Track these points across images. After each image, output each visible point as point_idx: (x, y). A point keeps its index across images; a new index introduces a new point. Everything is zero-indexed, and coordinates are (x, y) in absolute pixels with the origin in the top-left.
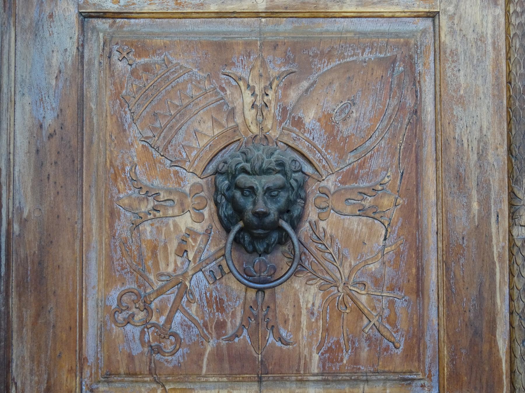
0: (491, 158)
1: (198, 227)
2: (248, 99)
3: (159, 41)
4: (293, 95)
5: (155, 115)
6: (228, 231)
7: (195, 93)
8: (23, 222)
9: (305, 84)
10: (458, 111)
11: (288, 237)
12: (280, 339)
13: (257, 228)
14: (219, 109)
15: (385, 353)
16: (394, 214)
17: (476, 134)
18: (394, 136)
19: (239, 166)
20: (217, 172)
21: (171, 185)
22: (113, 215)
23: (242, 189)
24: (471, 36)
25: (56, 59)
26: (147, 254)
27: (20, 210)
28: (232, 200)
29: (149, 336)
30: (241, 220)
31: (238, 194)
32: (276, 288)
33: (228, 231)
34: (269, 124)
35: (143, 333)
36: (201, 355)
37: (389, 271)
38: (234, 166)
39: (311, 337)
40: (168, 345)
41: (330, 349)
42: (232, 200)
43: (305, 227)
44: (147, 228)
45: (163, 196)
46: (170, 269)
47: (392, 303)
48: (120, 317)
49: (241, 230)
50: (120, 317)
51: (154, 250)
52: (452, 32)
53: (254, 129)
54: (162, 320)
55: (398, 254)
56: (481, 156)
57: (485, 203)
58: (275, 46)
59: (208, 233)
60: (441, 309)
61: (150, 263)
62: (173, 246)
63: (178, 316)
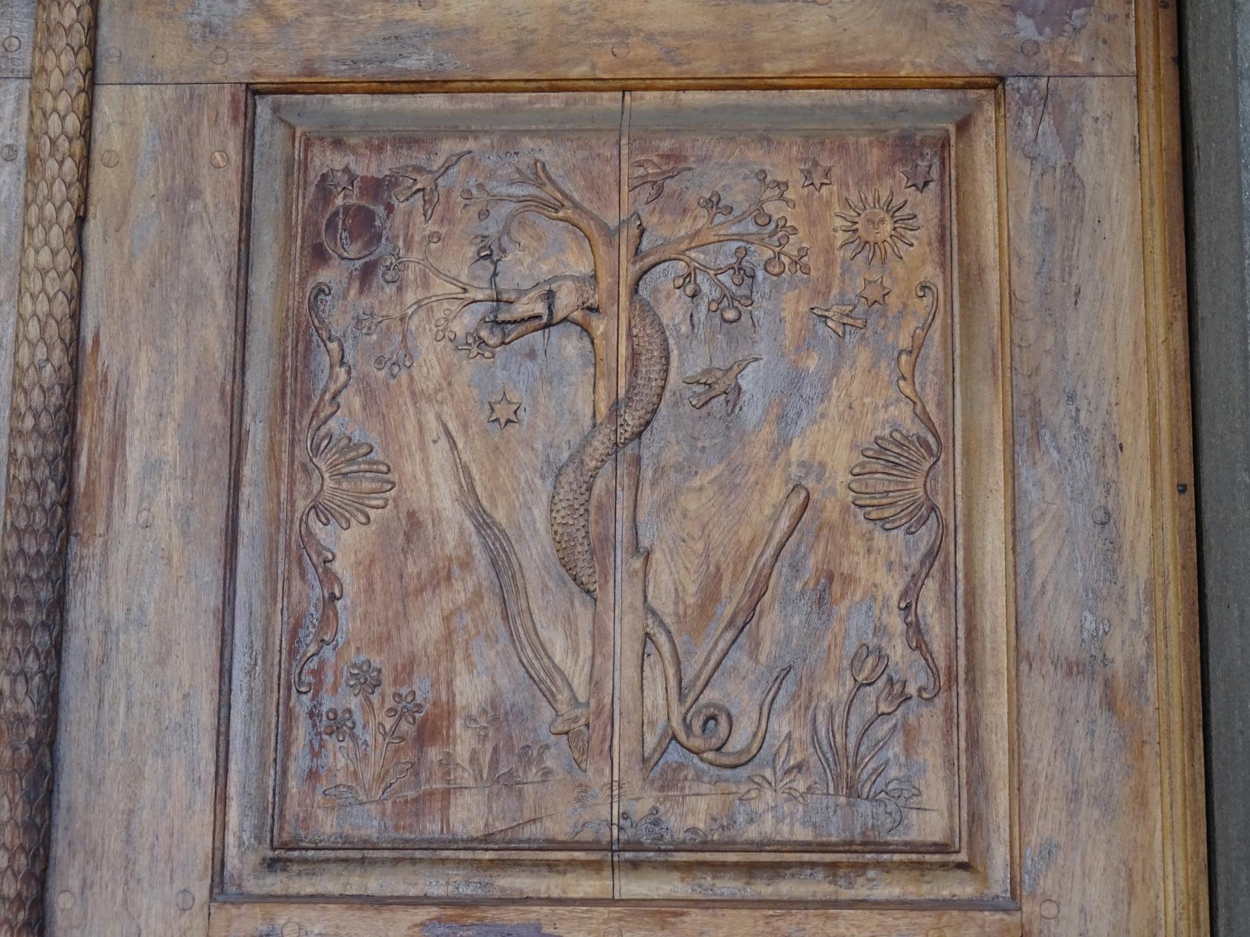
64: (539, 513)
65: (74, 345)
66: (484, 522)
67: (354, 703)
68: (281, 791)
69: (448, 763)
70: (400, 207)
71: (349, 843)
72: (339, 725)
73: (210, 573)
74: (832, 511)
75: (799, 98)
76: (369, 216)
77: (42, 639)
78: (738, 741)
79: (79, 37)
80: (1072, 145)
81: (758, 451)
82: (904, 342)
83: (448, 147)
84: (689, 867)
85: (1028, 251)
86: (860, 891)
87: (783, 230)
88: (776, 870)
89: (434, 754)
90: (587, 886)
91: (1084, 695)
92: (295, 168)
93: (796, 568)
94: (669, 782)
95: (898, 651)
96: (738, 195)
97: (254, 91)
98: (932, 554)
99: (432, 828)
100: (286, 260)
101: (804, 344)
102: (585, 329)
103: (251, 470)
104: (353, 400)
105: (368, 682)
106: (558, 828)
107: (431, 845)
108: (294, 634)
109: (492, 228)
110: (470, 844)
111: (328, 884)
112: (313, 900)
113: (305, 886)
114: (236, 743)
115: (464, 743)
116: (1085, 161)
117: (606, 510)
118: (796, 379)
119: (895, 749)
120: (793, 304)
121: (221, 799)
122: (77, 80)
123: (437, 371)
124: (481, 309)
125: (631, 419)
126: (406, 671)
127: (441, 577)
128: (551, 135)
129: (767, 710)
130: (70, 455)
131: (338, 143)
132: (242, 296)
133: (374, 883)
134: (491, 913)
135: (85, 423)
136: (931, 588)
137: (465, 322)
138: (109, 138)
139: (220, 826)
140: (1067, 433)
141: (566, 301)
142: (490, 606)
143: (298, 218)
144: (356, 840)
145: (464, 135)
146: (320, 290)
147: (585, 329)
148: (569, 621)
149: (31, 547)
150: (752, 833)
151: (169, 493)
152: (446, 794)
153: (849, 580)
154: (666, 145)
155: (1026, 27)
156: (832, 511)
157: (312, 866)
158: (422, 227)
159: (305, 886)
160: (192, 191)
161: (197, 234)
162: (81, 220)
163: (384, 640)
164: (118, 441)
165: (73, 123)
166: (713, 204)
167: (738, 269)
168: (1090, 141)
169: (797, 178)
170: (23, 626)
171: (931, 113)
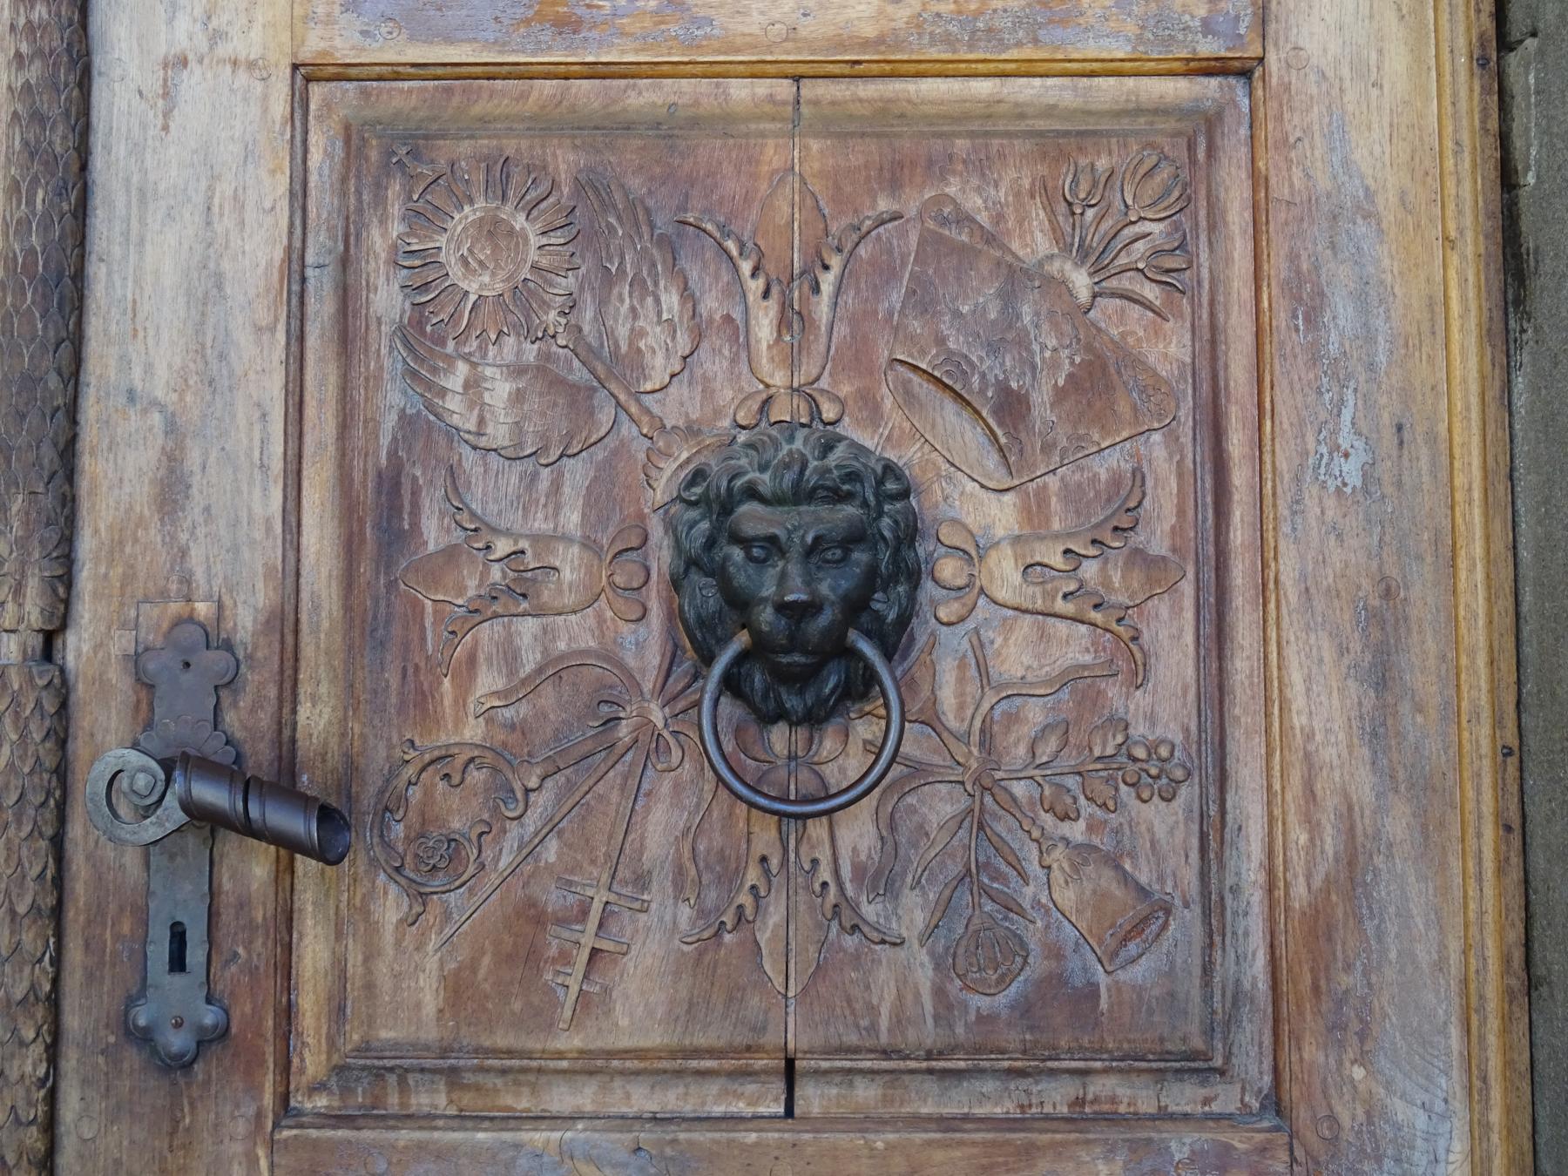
13: (787, 651)
15: (1419, 719)
19: (738, 483)
23: (745, 542)
30: (744, 627)
32: (810, 822)
38: (724, 484)
49: (742, 657)
60: (377, 68)
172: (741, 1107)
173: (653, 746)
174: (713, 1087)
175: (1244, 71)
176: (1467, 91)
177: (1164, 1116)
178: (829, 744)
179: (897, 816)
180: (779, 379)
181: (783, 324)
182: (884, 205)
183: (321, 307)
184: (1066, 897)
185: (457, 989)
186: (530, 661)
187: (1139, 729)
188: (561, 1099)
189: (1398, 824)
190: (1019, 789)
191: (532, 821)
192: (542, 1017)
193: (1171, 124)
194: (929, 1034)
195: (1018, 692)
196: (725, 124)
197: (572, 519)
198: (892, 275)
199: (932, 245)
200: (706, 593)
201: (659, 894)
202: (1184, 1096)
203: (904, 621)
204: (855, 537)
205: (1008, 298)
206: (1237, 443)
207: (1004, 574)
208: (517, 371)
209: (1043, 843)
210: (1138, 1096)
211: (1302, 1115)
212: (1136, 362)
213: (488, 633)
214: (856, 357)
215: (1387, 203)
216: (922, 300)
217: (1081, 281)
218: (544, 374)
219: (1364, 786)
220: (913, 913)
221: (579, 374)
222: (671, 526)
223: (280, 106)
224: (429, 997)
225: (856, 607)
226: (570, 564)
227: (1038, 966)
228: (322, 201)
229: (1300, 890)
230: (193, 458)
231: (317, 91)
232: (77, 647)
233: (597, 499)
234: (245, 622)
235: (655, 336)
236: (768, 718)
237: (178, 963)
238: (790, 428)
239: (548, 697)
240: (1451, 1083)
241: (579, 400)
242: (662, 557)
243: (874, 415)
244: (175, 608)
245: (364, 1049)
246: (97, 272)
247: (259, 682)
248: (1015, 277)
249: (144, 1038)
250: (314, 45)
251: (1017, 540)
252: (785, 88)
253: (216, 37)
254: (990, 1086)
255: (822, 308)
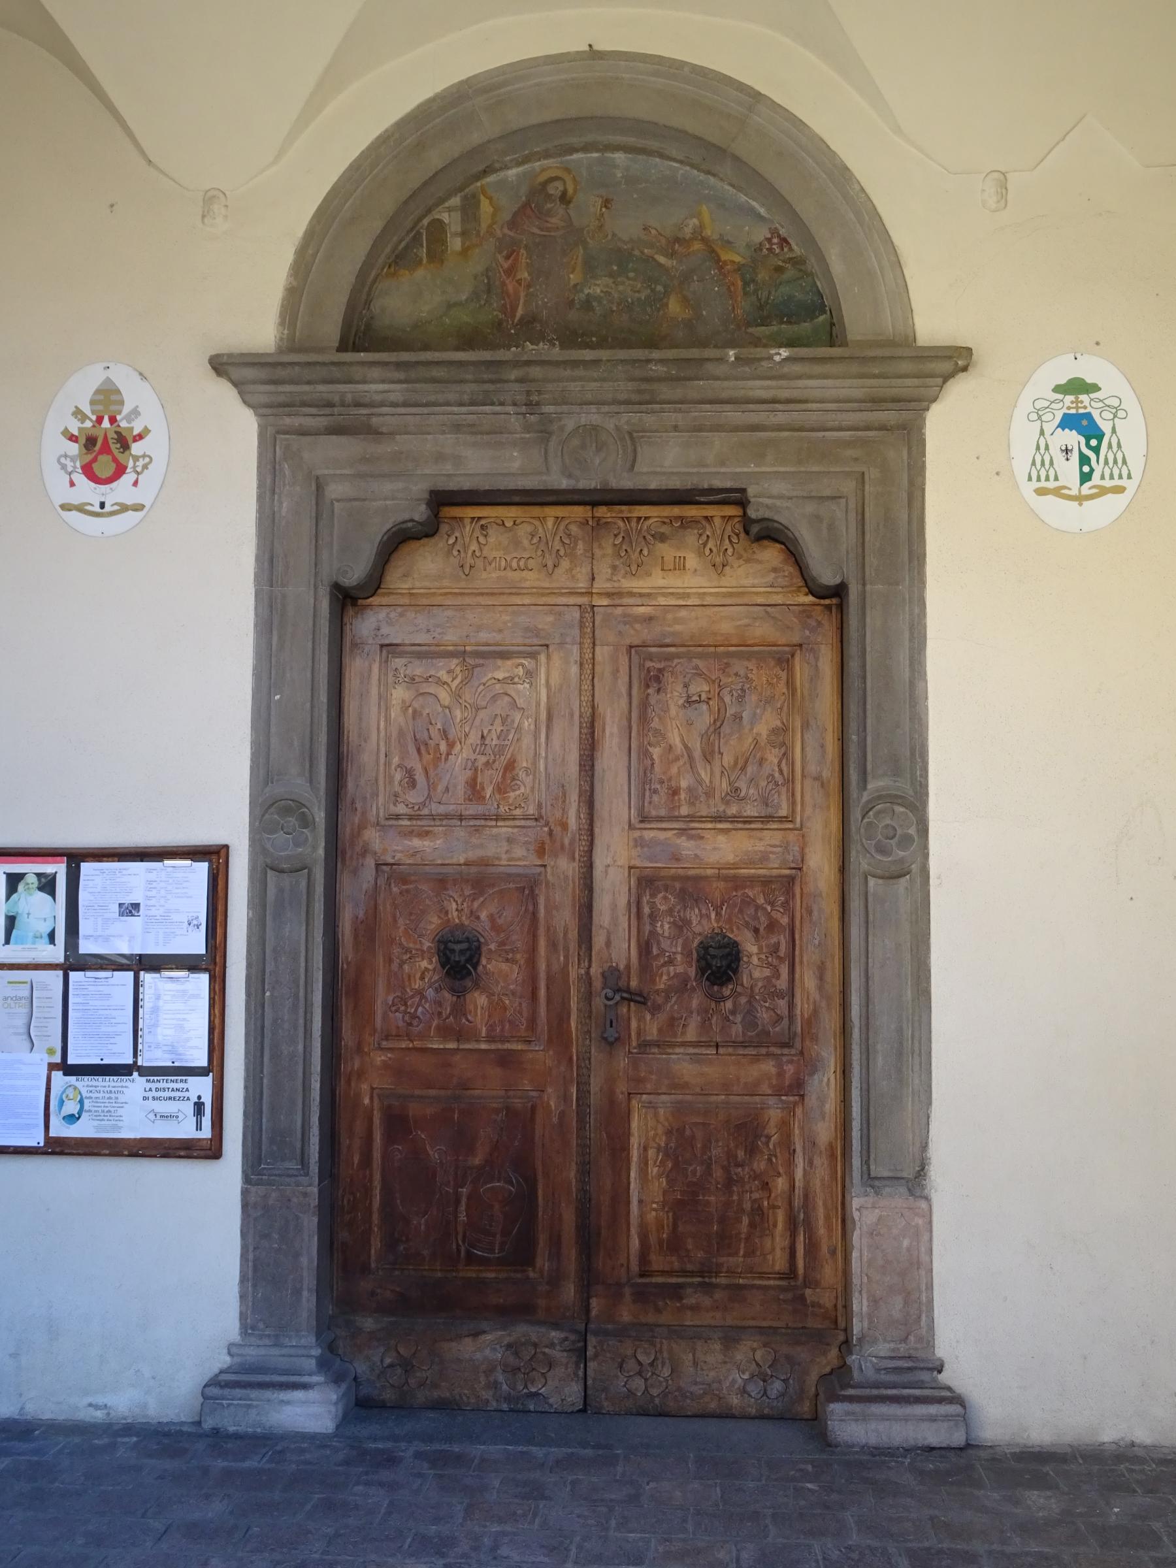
0: (570, 936)
1: (430, 967)
2: (454, 906)
3: (413, 878)
4: (476, 904)
5: (411, 914)
6: (444, 968)
7: (430, 903)
8: (348, 963)
9: (482, 899)
10: (554, 912)
11: (471, 973)
12: (468, 1020)
14: (441, 911)
16: (522, 962)
17: (563, 923)
18: (523, 925)
20: (439, 941)
21: (418, 946)
22: (390, 961)
24: (562, 877)
25: (365, 886)
26: (406, 979)
27: (347, 957)
28: (445, 954)
29: (407, 1018)
31: (448, 952)
33: (444, 968)
34: (464, 918)
35: (403, 1017)
36: (430, 1027)
37: (519, 988)
39: (482, 1019)
40: (415, 1022)
41: (491, 1026)
42: (445, 954)
43: (480, 968)
44: (406, 967)
45: (414, 952)
46: (417, 987)
47: (520, 1004)
48: (393, 1009)
50: (393, 1009)
51: (409, 977)
52: (553, 874)
53: (457, 921)
54: (413, 1010)
55: (524, 981)
56: (565, 934)
57: (566, 957)
58: (468, 881)
59: (434, 970)
61: (407, 983)
62: (418, 975)
63: (420, 1009)
64: (698, 744)
65: (593, 707)
66: (686, 747)
67: (658, 787)
68: (643, 806)
69: (679, 799)
70: (666, 675)
71: (658, 817)
72: (655, 791)
73: (626, 758)
74: (763, 744)
75: (756, 649)
76: (659, 678)
77: (590, 773)
78: (742, 794)
79: (591, 635)
80: (817, 659)
81: (746, 731)
82: (779, 706)
83: (676, 661)
84: (732, 822)
85: (807, 685)
86: (768, 827)
87: (752, 681)
88: (750, 822)
89: (676, 798)
90: (710, 826)
91: (817, 784)
92: (641, 666)
93: (755, 756)
94: (727, 803)
95: (777, 775)
96: (742, 672)
97: (631, 647)
98: (784, 754)
99: (676, 814)
100: (640, 688)
101: (757, 707)
102: (708, 703)
103: (634, 734)
104: (656, 719)
105: (662, 782)
106: (704, 814)
107: (677, 817)
108: (645, 773)
109: (687, 680)
110: (685, 817)
111: (653, 826)
112: (847, 1072)
113: (648, 826)
114: (632, 796)
115: (683, 796)
116: (820, 664)
117: (713, 745)
118: (755, 714)
119: (776, 796)
120: (754, 698)
121: (630, 808)
122: (591, 645)
123: (675, 713)
124: (685, 699)
125: (718, 724)
126: (670, 780)
127: (677, 759)
128: (700, 658)
129: (748, 788)
130: (593, 732)
131: (651, 660)
132: (630, 695)
133: (664, 825)
134: (690, 832)
135: (596, 724)
136: (784, 762)
137: (681, 702)
138: (598, 657)
139: (630, 813)
140: (814, 727)
141: (704, 697)
142: (688, 765)
143: (642, 676)
144: (814, 1031)
145: (679, 658)
146: (648, 694)
147: (708, 703)
148: (705, 768)
149: (586, 753)
150: (745, 814)
151: (615, 740)
152: (679, 807)
153: (766, 760)
154: (725, 661)
155: (807, 632)
156: (763, 744)
157: (650, 822)
158: (671, 680)
159: (648, 826)
160: (618, 671)
161: (620, 681)
162: (593, 678)
163: (664, 773)
164: (604, 730)
165: (591, 655)
166: (736, 674)
167: (742, 689)
168: (821, 659)
169: (755, 669)
170: (586, 771)
171: (786, 653)
172: (708, 1052)
173: (693, 989)
174: (703, 1049)
175: (800, 869)
176: (838, 875)
177: (783, 1055)
178: (724, 989)
179: (887, 874)
180: (716, 925)
181: (716, 915)
182: (734, 894)
183: (634, 910)
184: (765, 1016)
185: (660, 1030)
186: (672, 974)
187: (778, 987)
188: (677, 1050)
189: (824, 1004)
190: (757, 997)
191: (673, 1002)
192: (675, 1036)
193: (785, 879)
194: (741, 1039)
195: (758, 980)
196: (706, 878)
197: (679, 949)
198: (736, 906)
199: (743, 901)
200: (703, 963)
201: (695, 1015)
202: (786, 1051)
203: (737, 967)
204: (729, 954)
205: (756, 911)
206: (797, 937)
207: (755, 960)
208: (669, 923)
209: (762, 1006)
210: (777, 1051)
211: (806, 1054)
212: (778, 922)
213: (665, 969)
214: (729, 921)
215: (824, 895)
216: (741, 911)
217: (769, 908)
218: (674, 924)
219: (818, 997)
220: (739, 1018)
221: (681, 923)
222: (698, 953)
223: (626, 874)
224: (655, 1031)
225: (729, 966)
226: (679, 957)
227: (760, 1028)
228: (634, 891)
229: (806, 1016)
230: (612, 938)
231: (632, 871)
232: (593, 971)
233: (684, 946)
234: (622, 967)
235: (694, 917)
236: (714, 984)
237: (611, 1026)
238: (717, 934)
239: (675, 980)
240: (832, 1049)
241: (680, 928)
242: (695, 955)
243: (732, 932)
244: (609, 964)
245: (644, 1041)
246: (595, 904)
247: (624, 978)
248: (758, 907)
249: (605, 1039)
250: (633, 863)
251: (757, 954)
252: (717, 871)
253: (615, 861)
254: (752, 1049)
255: (723, 912)
